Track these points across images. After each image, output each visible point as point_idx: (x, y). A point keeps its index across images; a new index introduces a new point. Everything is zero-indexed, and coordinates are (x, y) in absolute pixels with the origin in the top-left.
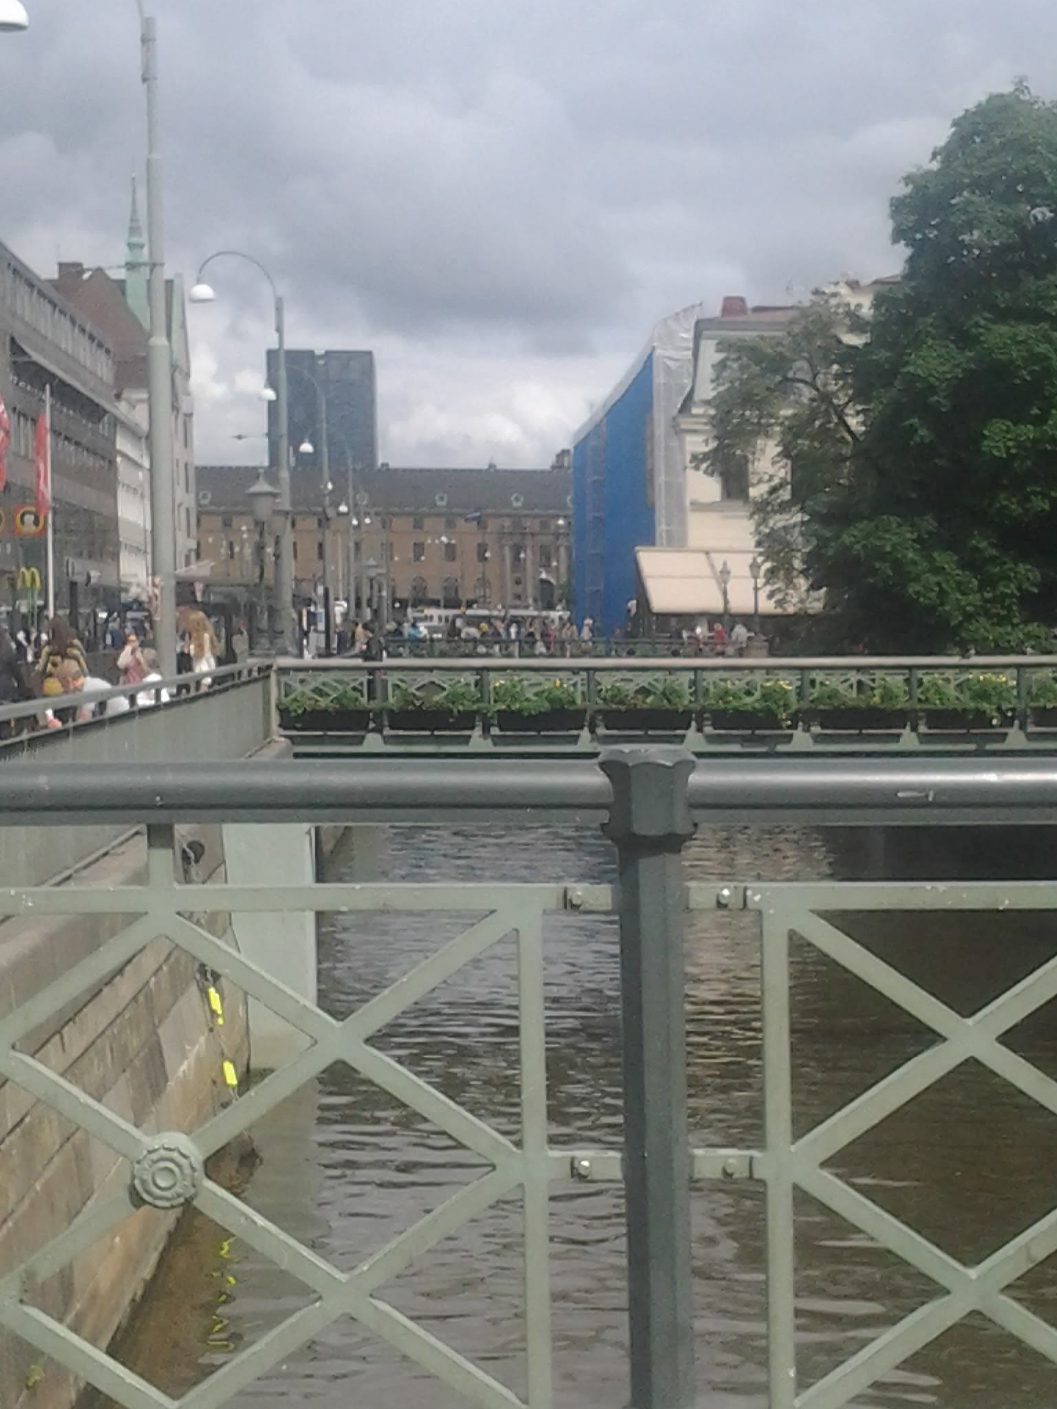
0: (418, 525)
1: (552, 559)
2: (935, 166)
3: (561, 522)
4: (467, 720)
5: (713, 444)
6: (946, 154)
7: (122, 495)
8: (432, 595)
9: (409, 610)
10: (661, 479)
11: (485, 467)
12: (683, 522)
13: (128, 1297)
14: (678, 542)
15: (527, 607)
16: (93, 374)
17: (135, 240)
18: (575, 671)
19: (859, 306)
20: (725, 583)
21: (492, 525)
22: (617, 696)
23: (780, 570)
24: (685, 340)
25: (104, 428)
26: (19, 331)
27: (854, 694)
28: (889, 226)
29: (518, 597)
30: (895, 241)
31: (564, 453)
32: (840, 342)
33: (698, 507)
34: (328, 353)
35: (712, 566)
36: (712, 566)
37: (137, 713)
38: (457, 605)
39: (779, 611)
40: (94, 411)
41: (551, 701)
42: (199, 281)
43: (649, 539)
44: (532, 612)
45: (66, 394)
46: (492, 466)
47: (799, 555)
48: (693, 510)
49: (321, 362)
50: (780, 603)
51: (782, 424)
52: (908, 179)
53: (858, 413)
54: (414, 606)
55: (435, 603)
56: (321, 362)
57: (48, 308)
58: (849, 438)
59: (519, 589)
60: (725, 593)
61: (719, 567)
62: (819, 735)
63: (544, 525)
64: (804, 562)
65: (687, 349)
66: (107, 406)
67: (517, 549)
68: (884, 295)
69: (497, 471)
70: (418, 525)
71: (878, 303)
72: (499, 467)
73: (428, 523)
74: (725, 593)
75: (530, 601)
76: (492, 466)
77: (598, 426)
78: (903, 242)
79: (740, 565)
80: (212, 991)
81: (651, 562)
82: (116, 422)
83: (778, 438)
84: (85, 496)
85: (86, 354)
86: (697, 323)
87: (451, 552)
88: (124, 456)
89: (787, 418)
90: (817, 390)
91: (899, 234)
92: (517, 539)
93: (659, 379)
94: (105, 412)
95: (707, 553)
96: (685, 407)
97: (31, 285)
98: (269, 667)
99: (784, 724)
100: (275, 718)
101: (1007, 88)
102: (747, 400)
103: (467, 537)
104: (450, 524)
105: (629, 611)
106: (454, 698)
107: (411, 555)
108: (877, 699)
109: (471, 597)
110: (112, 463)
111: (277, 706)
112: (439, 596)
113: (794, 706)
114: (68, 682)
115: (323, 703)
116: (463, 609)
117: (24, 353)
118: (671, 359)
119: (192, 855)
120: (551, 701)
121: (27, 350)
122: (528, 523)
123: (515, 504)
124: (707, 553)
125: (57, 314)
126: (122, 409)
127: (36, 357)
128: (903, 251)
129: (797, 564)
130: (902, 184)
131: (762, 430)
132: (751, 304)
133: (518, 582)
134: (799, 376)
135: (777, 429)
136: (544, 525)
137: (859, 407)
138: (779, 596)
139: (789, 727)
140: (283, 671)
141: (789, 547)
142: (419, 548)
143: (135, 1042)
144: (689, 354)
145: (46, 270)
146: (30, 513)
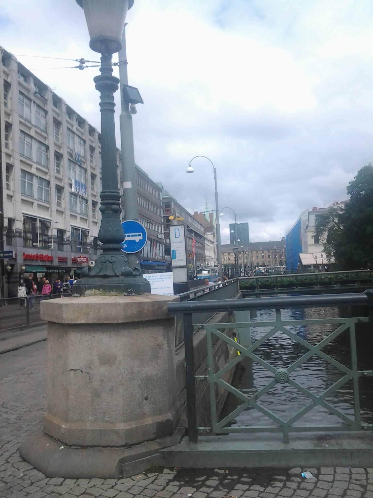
0: (257, 252)
1: (282, 256)
2: (355, 180)
3: (284, 250)
4: (274, 287)
5: (315, 234)
6: (357, 178)
7: (206, 251)
8: (260, 265)
9: (256, 268)
10: (303, 241)
11: (269, 241)
12: (307, 248)
13: (226, 396)
14: (307, 252)
15: (278, 266)
16: (201, 230)
17: (207, 207)
18: (293, 276)
19: (342, 206)
20: (316, 259)
21: (271, 251)
22: (302, 281)
23: (329, 256)
24: (306, 215)
25: (202, 239)
26: (188, 224)
27: (345, 278)
28: (347, 191)
29: (276, 264)
30: (348, 194)
31: (284, 237)
32: (338, 213)
33: (310, 245)
34: (240, 224)
35: (313, 256)
36: (313, 256)
37: (219, 288)
38: (265, 266)
39: (329, 263)
40: (201, 237)
41: (289, 282)
42: (221, 213)
43: (301, 252)
44: (279, 266)
45: (197, 234)
46: (270, 241)
47: (333, 253)
48: (309, 246)
49: (239, 225)
50: (329, 262)
51: (328, 229)
52: (350, 183)
53: (342, 226)
54: (257, 267)
55: (261, 266)
56: (239, 225)
57: (193, 220)
58: (341, 231)
59: (276, 263)
60: (316, 261)
61: (315, 256)
62: (360, 285)
63: (280, 251)
64: (334, 254)
65: (307, 217)
66: (203, 235)
67: (275, 255)
68: (347, 205)
69: (271, 242)
70: (257, 252)
71: (346, 206)
72: (271, 241)
73: (259, 252)
74: (316, 261)
75: (278, 264)
76: (270, 241)
77: (290, 232)
78: (349, 195)
79: (319, 255)
80: (235, 338)
81: (302, 256)
82: (205, 238)
83: (328, 232)
84: (200, 251)
85: (199, 227)
86: (309, 212)
87: (263, 257)
88: (206, 244)
89: (329, 228)
90: (334, 222)
91: (348, 193)
92: (275, 254)
93: (302, 223)
94: (203, 236)
95: (312, 253)
96: (307, 228)
97: (190, 216)
98: (238, 279)
99: (333, 284)
100: (239, 288)
101: (367, 165)
102: (322, 225)
103: (266, 253)
104: (263, 252)
105: (298, 265)
106: (271, 283)
107: (256, 258)
108: (350, 279)
109: (267, 264)
110: (204, 245)
111: (239, 286)
112: (262, 265)
113: (335, 281)
114: (256, 282)
115: (247, 285)
116: (266, 267)
117: (189, 227)
118: (304, 219)
119: (230, 314)
120: (289, 282)
121: (190, 227)
122: (277, 251)
123: (275, 247)
124: (312, 253)
125: (194, 221)
126: (205, 236)
127: (191, 228)
128: (350, 196)
129: (332, 254)
130: (349, 184)
131: (325, 230)
132: (318, 208)
133: (276, 261)
134: (331, 220)
135: (327, 230)
136: (280, 251)
137: (343, 225)
138: (328, 260)
139: (334, 285)
140: (240, 279)
141: (331, 251)
142: (258, 257)
143: (224, 348)
144: (307, 218)
145: (192, 213)
146: (191, 254)
